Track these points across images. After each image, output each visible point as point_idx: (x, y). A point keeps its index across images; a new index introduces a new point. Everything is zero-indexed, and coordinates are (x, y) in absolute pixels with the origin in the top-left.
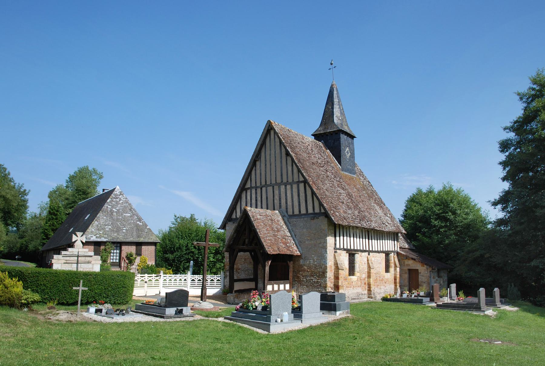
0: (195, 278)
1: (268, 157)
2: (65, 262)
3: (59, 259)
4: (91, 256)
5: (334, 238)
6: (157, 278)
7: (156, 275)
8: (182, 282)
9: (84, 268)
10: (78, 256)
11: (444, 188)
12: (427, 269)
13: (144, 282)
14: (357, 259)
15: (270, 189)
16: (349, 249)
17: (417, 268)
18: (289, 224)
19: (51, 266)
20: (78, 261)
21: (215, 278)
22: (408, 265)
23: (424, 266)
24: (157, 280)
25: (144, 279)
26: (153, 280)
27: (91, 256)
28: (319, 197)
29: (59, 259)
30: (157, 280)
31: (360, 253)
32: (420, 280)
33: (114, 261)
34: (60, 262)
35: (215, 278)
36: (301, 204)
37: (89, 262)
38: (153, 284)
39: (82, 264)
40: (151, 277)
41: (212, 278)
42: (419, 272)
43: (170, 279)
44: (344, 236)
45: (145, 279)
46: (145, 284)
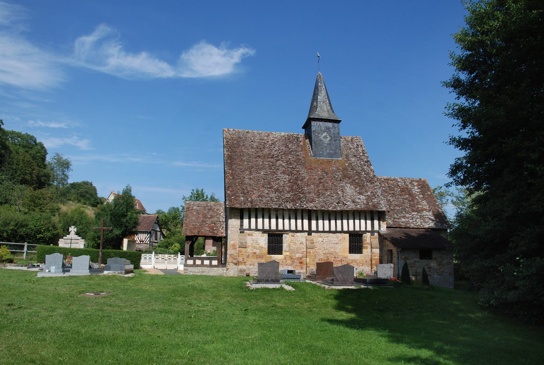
0: (159, 257)
2: (65, 243)
3: (62, 241)
4: (79, 240)
5: (282, 220)
6: (176, 257)
7: (174, 255)
8: (147, 260)
9: (74, 246)
10: (71, 240)
11: (71, 165)
13: (164, 260)
14: (266, 243)
16: (273, 231)
19: (58, 245)
20: (71, 242)
21: (148, 256)
24: (175, 259)
25: (164, 258)
26: (172, 259)
27: (79, 240)
29: (62, 241)
30: (175, 259)
31: (291, 234)
34: (62, 242)
35: (148, 256)
37: (77, 243)
38: (160, 261)
39: (74, 244)
40: (164, 256)
41: (150, 257)
43: (145, 257)
44: (272, 216)
45: (165, 257)
46: (166, 261)
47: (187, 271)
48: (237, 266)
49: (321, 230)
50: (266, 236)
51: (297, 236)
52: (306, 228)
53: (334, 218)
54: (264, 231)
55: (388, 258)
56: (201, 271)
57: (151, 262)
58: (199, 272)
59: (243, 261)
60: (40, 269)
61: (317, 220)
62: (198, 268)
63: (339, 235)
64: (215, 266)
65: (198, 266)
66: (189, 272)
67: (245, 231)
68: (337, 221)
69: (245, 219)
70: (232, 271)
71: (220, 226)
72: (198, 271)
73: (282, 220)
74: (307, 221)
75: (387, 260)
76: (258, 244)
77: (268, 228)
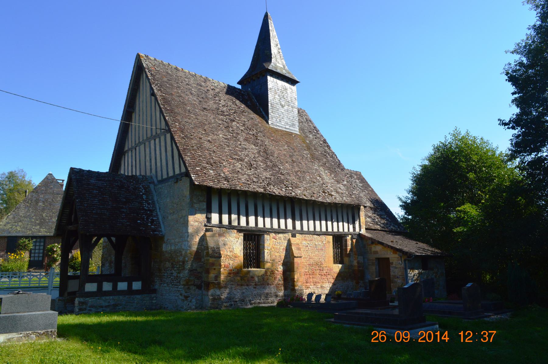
1: (141, 105)
12: (401, 257)
15: (142, 147)
17: (388, 256)
18: (155, 193)
22: (376, 252)
23: (396, 253)
28: (181, 148)
31: (273, 235)
32: (392, 274)
33: (36, 259)
36: (168, 162)
42: (391, 261)
47: (84, 307)
48: (200, 292)
49: (305, 230)
50: (241, 236)
51: (280, 238)
52: (290, 227)
53: (236, 212)
54: (240, 230)
55: (376, 269)
56: (113, 303)
57: (47, 288)
58: (108, 306)
59: (216, 282)
60: (422, 339)
61: (301, 220)
62: (108, 298)
63: (323, 237)
64: (137, 292)
65: (107, 293)
66: (90, 307)
67: (214, 229)
68: (339, 223)
69: (224, 214)
70: (193, 300)
71: (147, 219)
72: (107, 304)
73: (262, 219)
74: (331, 222)
75: (30, 261)
76: (231, 251)
77: (262, 226)
